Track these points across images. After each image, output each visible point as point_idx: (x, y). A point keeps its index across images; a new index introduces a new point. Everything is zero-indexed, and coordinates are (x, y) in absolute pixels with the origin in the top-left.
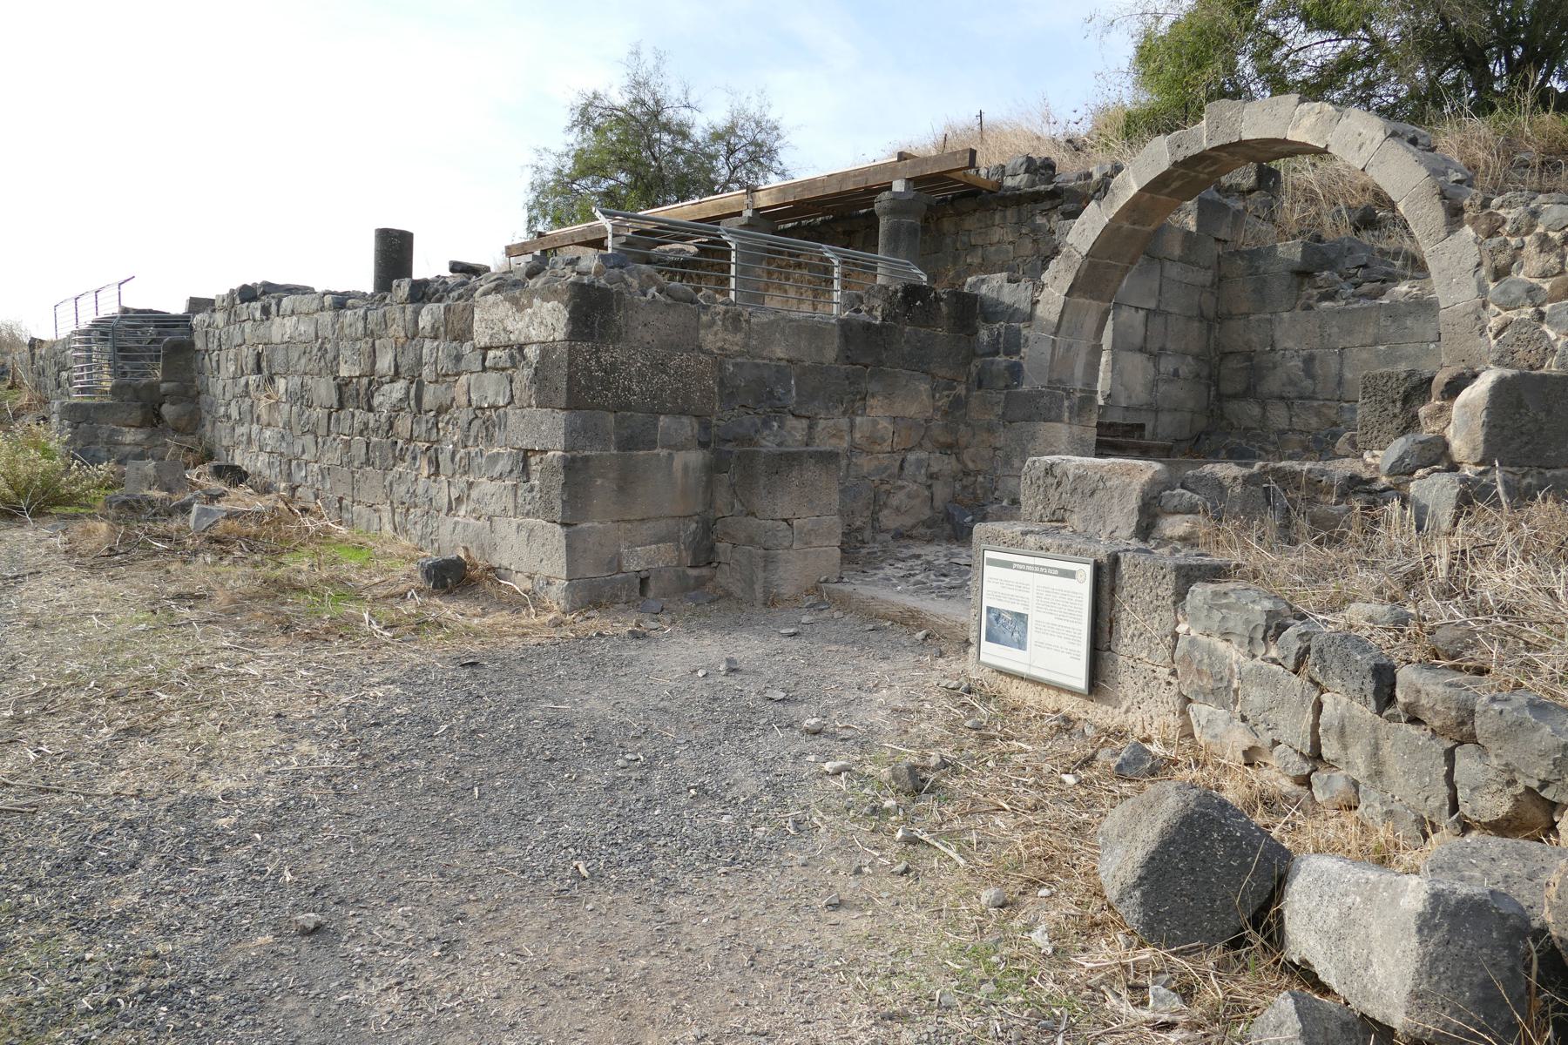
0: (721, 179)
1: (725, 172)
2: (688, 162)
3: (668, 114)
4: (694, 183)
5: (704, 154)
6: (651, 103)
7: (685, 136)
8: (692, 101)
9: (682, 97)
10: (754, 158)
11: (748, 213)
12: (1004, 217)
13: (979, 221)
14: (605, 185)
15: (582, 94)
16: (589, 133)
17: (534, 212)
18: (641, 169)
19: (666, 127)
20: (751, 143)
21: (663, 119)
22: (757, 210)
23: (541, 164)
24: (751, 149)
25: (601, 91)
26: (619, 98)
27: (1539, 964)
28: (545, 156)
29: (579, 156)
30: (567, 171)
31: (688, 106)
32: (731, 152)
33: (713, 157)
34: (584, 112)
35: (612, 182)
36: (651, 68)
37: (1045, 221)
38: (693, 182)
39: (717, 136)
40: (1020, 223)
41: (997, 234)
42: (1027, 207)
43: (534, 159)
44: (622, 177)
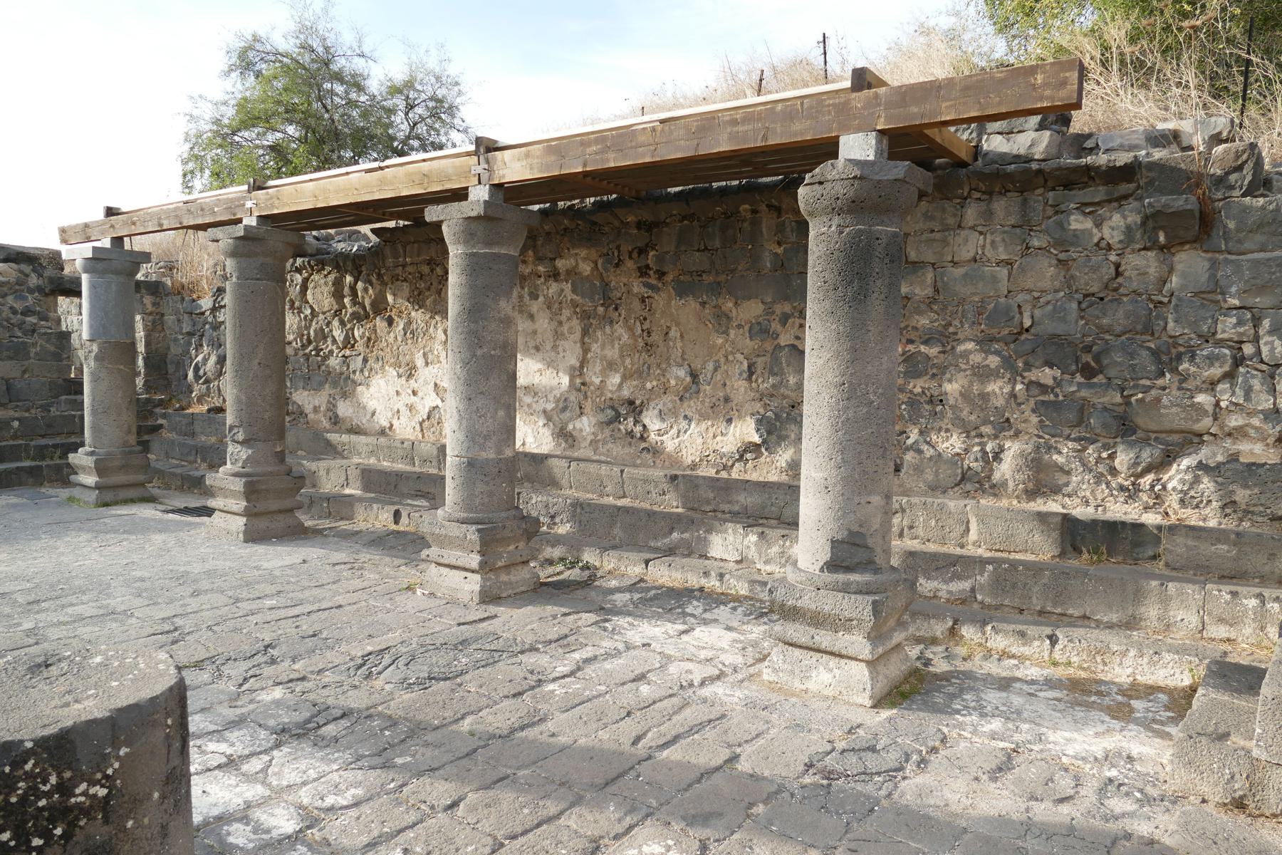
0: (401, 135)
1: (405, 127)
2: (365, 115)
3: (339, 64)
4: (371, 137)
5: (383, 108)
6: (320, 50)
7: (360, 88)
8: (366, 49)
9: (355, 46)
10: (435, 115)
11: (480, 194)
12: (988, 215)
13: (928, 217)
14: (271, 138)
15: (240, 36)
16: (251, 79)
17: (191, 166)
18: (312, 121)
19: (338, 77)
20: (431, 99)
21: (334, 67)
22: (497, 187)
23: (196, 113)
24: (431, 104)
25: (262, 33)
26: (283, 40)
27: (498, 244)
28: (201, 104)
29: (242, 105)
30: (226, 121)
31: (362, 55)
32: (410, 107)
33: (391, 111)
34: (243, 54)
35: (279, 135)
36: (318, 11)
37: (1088, 224)
38: (362, 136)
39: (395, 90)
40: (1025, 225)
41: (968, 245)
42: (1038, 198)
43: (188, 107)
44: (291, 130)
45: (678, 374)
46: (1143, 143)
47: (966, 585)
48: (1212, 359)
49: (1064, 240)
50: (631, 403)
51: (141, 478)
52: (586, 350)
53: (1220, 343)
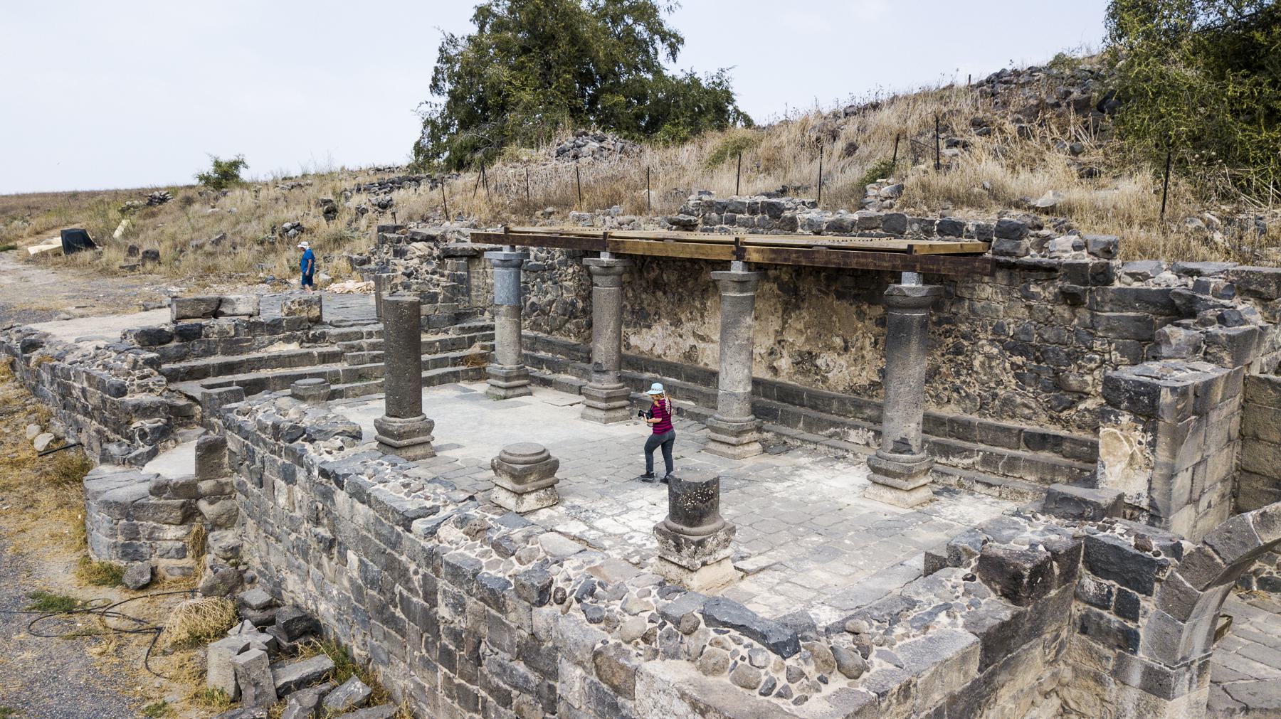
45: (838, 341)
46: (1070, 248)
47: (970, 461)
48: (1091, 360)
49: (1029, 296)
50: (810, 353)
51: (525, 381)
52: (785, 322)
53: (1096, 352)
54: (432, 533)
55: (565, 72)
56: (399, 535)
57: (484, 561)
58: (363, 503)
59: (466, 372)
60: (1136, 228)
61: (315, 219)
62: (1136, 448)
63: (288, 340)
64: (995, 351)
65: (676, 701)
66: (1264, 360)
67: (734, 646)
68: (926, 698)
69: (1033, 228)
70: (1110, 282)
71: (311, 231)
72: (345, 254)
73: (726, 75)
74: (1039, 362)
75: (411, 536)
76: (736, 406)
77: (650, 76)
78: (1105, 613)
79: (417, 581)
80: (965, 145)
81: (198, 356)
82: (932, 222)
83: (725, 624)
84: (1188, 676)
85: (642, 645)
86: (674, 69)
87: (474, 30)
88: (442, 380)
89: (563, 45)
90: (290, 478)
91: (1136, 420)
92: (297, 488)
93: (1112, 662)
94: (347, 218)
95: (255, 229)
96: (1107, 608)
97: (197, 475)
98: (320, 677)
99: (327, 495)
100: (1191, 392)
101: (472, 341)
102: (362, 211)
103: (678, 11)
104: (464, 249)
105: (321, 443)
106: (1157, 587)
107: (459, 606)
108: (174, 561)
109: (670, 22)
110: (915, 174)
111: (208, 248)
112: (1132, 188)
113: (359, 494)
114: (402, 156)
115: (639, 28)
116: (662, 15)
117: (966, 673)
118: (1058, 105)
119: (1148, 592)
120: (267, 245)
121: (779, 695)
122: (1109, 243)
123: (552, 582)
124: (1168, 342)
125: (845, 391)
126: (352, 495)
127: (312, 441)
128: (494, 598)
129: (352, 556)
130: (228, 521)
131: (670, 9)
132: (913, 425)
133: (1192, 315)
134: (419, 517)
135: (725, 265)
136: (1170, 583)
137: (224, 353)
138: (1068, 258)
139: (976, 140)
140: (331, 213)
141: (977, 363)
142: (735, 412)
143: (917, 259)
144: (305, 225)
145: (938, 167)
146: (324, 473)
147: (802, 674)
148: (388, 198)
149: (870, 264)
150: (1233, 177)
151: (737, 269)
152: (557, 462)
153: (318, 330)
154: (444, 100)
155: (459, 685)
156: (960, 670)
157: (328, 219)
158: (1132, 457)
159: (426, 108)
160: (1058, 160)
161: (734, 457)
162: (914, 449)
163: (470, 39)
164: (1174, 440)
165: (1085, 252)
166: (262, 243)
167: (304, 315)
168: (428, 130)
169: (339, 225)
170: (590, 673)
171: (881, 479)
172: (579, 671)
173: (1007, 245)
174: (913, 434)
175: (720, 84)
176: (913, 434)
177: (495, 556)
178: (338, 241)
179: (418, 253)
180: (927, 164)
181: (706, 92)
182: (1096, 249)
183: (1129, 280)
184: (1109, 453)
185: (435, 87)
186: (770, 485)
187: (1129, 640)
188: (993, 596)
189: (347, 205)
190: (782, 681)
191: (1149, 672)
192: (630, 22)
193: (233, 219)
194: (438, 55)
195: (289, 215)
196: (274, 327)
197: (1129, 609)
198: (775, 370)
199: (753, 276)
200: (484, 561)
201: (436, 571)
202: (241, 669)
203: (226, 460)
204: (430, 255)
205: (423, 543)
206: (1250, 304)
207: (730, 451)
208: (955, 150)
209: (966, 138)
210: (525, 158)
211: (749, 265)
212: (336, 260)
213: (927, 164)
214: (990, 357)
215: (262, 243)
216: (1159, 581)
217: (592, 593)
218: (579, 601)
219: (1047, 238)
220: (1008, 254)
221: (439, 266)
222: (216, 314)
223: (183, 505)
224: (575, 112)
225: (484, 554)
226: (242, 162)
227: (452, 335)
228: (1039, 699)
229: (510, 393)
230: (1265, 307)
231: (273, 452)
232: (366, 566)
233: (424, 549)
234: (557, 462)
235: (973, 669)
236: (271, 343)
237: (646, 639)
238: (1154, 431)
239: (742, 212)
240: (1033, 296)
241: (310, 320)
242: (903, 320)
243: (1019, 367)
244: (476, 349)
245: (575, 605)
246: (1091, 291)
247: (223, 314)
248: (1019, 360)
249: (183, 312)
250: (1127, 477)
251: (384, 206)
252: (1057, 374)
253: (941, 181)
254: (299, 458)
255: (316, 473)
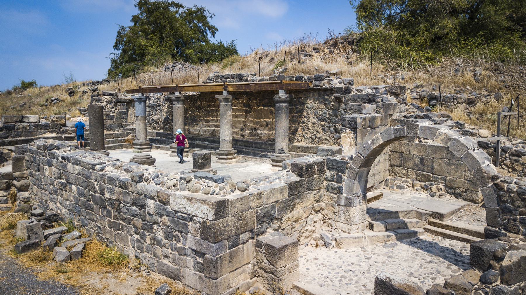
54: (102, 169)
55: (169, 40)
56: (91, 172)
57: (121, 175)
58: (77, 165)
59: (126, 145)
60: (362, 78)
61: (65, 96)
62: (352, 140)
63: (51, 132)
64: (315, 121)
65: (183, 200)
66: (397, 114)
67: (203, 183)
68: (268, 199)
69: (327, 77)
70: (350, 93)
71: (63, 101)
72: (78, 108)
73: (234, 43)
74: (329, 123)
75: (95, 171)
76: (226, 144)
77: (204, 43)
78: (333, 183)
79: (97, 188)
80: (310, 56)
81: (13, 137)
82: (293, 77)
83: (201, 177)
84: (358, 200)
85: (173, 188)
86: (213, 41)
87: (132, 24)
88: (116, 148)
89: (168, 29)
90: (50, 165)
91: (351, 130)
92: (53, 167)
93: (336, 199)
94: (79, 95)
95: (41, 100)
96: (333, 181)
97: (12, 170)
98: (61, 232)
99: (65, 166)
100: (367, 120)
101: (128, 134)
102: (85, 93)
103: (214, 17)
104: (125, 99)
105: (62, 149)
106: (347, 171)
107: (112, 192)
108: (3, 205)
109: (212, 22)
110: (290, 65)
111: (19, 108)
112: (363, 66)
113: (76, 162)
114: (104, 76)
115: (200, 25)
116: (209, 19)
117: (283, 195)
118: (343, 43)
119: (344, 173)
120: (44, 107)
121: (217, 194)
122: (350, 80)
123: (144, 175)
124: (365, 108)
125: (267, 141)
126: (73, 164)
127: (59, 149)
128: (124, 186)
129: (74, 188)
130: (25, 188)
131: (211, 17)
132: (285, 144)
133: (374, 101)
134: (98, 165)
135: (221, 93)
136: (351, 168)
137: (24, 136)
138: (338, 85)
139: (314, 53)
140: (72, 93)
141: (310, 126)
142: (226, 146)
143: (284, 85)
144: (61, 98)
145: (299, 62)
146: (63, 158)
147: (224, 188)
148: (96, 87)
149: (269, 88)
150: (396, 63)
151: (225, 94)
152: (155, 159)
153: (64, 129)
154: (119, 52)
155: (113, 222)
156: (280, 194)
157: (70, 96)
158: (351, 143)
159: (112, 56)
160: (342, 60)
161: (226, 163)
162: (286, 152)
163: (130, 28)
164: (362, 135)
165: (343, 84)
166: (42, 106)
167: (59, 122)
168: (114, 65)
169: (76, 98)
170: (156, 201)
171: (275, 164)
172: (153, 201)
173: (317, 83)
174: (285, 147)
175: (232, 46)
176: (285, 147)
177: (125, 173)
178: (75, 104)
179: (106, 100)
180: (295, 62)
181: (226, 49)
182: (346, 82)
183: (356, 92)
184: (344, 143)
185: (116, 47)
186: (237, 169)
187: (339, 191)
188: (295, 176)
189: (79, 90)
190: (217, 190)
191: (347, 199)
192: (196, 22)
193: (29, 98)
194: (117, 34)
195: (54, 95)
196: (46, 127)
197: (339, 180)
198: (243, 136)
199: (230, 97)
200: (121, 175)
201: (104, 182)
202: (30, 228)
203: (25, 164)
204: (111, 101)
205: (99, 173)
206: (392, 97)
207: (225, 161)
208: (306, 57)
209: (311, 53)
210: (152, 71)
211: (229, 93)
212: (73, 111)
213: (295, 62)
214: (313, 123)
215: (42, 106)
216: (347, 168)
217: (158, 177)
218: (153, 179)
219: (331, 80)
220: (318, 86)
221: (115, 105)
222: (21, 121)
223: (6, 182)
224: (174, 56)
225: (121, 173)
226: (35, 83)
227: (120, 131)
228: (313, 212)
229: (142, 150)
230: (397, 98)
231: (43, 156)
232: (79, 189)
233: (100, 175)
234: (155, 159)
235: (286, 195)
236: (45, 133)
237: (174, 186)
238: (356, 133)
239: (229, 78)
240: (326, 100)
241: (61, 125)
242: (279, 107)
243: (323, 126)
244: (130, 137)
245: (152, 181)
246: (344, 97)
247: (24, 122)
248: (323, 123)
249: (7, 121)
250: (350, 150)
251: (94, 91)
252: (335, 127)
253: (300, 67)
254: (54, 156)
255: (60, 159)
